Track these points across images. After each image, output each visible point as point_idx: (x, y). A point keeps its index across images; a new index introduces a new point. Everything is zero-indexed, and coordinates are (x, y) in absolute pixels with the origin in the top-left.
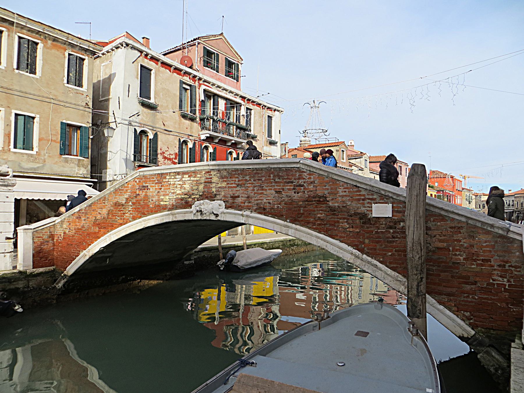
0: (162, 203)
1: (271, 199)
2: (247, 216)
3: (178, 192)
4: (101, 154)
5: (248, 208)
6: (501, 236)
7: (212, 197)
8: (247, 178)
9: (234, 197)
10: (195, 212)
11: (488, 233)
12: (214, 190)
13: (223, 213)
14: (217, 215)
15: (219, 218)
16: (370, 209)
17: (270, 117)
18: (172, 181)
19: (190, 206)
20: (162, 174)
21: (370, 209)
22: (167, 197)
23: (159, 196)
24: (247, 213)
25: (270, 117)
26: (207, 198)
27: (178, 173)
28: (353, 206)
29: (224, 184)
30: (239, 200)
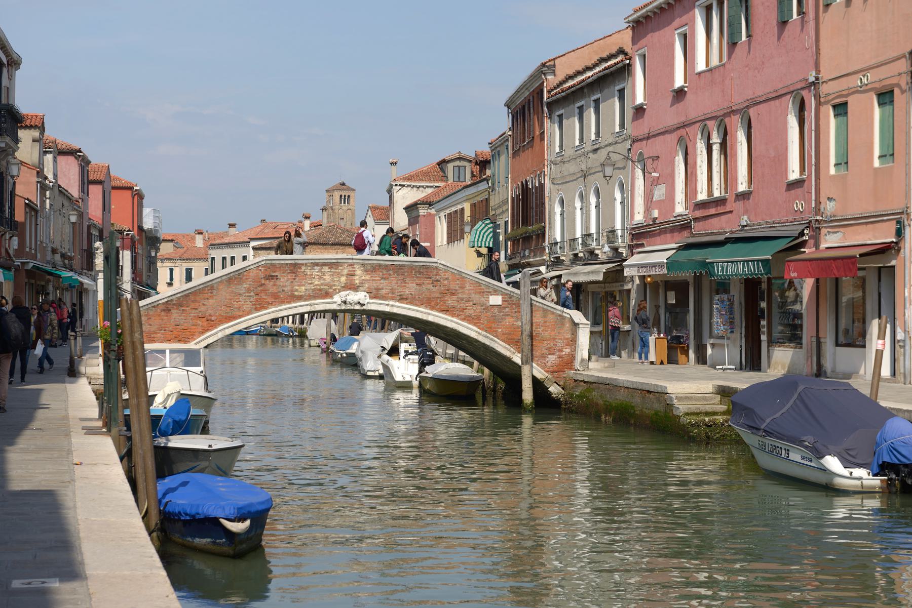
0: (296, 293)
1: (413, 291)
2: (392, 306)
3: (316, 283)
4: (583, 92)
5: (393, 299)
6: (560, 316)
7: (355, 288)
8: (391, 272)
9: (378, 289)
10: (340, 302)
11: (553, 313)
12: (357, 282)
13: (369, 303)
14: (363, 305)
15: (364, 307)
16: (306, 316)
17: (171, 270)
18: (308, 272)
19: (332, 297)
20: (296, 264)
21: (291, 318)
22: (303, 288)
23: (293, 287)
24: (391, 303)
25: (171, 270)
26: (350, 289)
27: (317, 264)
28: (476, 297)
29: (368, 277)
30: (383, 292)
